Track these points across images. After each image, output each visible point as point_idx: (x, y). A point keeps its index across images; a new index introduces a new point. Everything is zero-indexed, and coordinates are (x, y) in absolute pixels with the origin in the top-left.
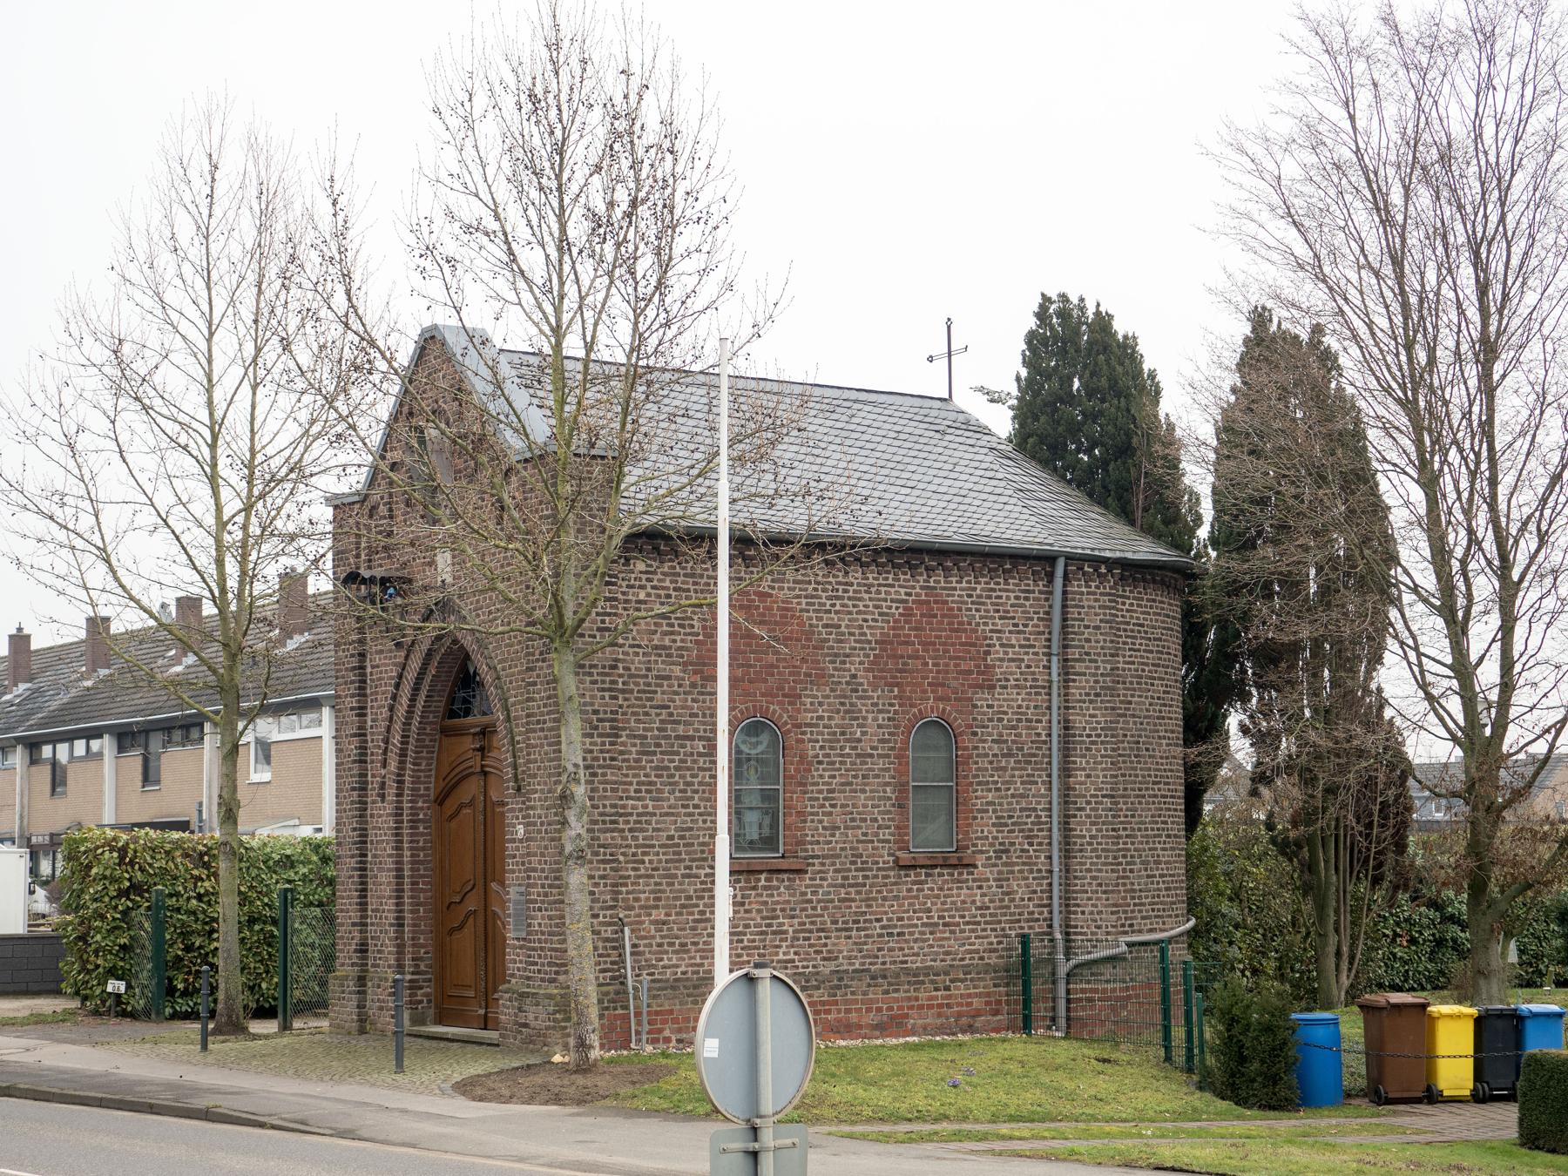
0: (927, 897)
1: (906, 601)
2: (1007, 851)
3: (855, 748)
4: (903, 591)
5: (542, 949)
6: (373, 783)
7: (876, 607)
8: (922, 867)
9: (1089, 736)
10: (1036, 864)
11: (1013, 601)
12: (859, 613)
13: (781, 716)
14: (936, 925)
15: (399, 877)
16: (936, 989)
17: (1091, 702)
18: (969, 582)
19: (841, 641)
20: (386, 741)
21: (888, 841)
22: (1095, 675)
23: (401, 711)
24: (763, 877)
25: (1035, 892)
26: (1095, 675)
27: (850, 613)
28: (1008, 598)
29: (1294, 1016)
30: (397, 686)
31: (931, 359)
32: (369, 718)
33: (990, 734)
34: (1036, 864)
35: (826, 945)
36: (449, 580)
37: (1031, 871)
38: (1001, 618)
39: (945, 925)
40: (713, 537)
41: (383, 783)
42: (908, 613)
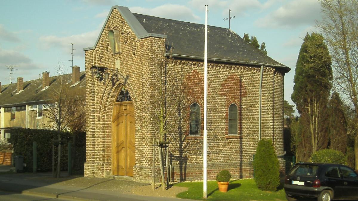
0: (232, 146)
1: (228, 75)
2: (249, 135)
3: (217, 110)
4: (227, 73)
5: (146, 157)
6: (96, 117)
7: (221, 77)
8: (231, 138)
9: (267, 108)
10: (255, 138)
11: (251, 76)
12: (218, 78)
13: (200, 102)
14: (234, 152)
15: (241, 123)
16: (234, 167)
17: (268, 100)
18: (242, 71)
19: (214, 85)
20: (100, 107)
21: (223, 132)
22: (269, 94)
23: (104, 100)
24: (196, 140)
25: (255, 145)
26: (269, 94)
27: (216, 78)
28: (250, 75)
29: (295, 183)
30: (104, 94)
31: (225, 19)
32: (95, 102)
33: (246, 107)
34: (255, 138)
35: (210, 157)
36: (119, 68)
37: (254, 140)
38: (249, 80)
39: (236, 152)
40: (210, 61)
41: (99, 117)
42: (229, 78)
